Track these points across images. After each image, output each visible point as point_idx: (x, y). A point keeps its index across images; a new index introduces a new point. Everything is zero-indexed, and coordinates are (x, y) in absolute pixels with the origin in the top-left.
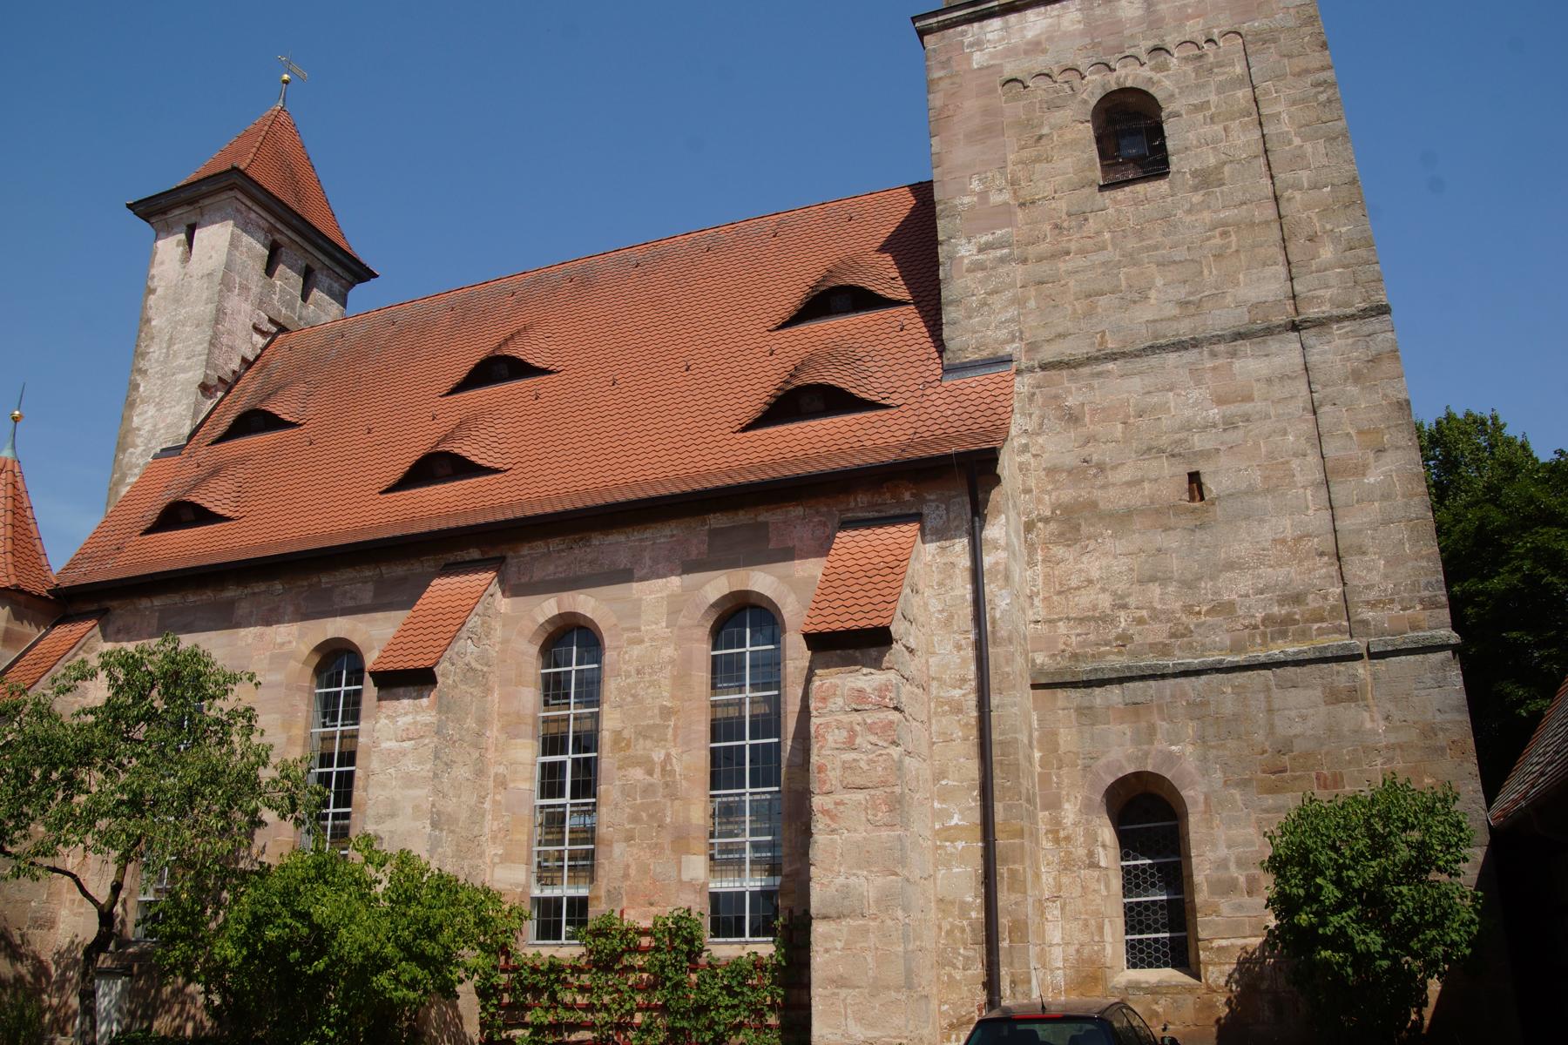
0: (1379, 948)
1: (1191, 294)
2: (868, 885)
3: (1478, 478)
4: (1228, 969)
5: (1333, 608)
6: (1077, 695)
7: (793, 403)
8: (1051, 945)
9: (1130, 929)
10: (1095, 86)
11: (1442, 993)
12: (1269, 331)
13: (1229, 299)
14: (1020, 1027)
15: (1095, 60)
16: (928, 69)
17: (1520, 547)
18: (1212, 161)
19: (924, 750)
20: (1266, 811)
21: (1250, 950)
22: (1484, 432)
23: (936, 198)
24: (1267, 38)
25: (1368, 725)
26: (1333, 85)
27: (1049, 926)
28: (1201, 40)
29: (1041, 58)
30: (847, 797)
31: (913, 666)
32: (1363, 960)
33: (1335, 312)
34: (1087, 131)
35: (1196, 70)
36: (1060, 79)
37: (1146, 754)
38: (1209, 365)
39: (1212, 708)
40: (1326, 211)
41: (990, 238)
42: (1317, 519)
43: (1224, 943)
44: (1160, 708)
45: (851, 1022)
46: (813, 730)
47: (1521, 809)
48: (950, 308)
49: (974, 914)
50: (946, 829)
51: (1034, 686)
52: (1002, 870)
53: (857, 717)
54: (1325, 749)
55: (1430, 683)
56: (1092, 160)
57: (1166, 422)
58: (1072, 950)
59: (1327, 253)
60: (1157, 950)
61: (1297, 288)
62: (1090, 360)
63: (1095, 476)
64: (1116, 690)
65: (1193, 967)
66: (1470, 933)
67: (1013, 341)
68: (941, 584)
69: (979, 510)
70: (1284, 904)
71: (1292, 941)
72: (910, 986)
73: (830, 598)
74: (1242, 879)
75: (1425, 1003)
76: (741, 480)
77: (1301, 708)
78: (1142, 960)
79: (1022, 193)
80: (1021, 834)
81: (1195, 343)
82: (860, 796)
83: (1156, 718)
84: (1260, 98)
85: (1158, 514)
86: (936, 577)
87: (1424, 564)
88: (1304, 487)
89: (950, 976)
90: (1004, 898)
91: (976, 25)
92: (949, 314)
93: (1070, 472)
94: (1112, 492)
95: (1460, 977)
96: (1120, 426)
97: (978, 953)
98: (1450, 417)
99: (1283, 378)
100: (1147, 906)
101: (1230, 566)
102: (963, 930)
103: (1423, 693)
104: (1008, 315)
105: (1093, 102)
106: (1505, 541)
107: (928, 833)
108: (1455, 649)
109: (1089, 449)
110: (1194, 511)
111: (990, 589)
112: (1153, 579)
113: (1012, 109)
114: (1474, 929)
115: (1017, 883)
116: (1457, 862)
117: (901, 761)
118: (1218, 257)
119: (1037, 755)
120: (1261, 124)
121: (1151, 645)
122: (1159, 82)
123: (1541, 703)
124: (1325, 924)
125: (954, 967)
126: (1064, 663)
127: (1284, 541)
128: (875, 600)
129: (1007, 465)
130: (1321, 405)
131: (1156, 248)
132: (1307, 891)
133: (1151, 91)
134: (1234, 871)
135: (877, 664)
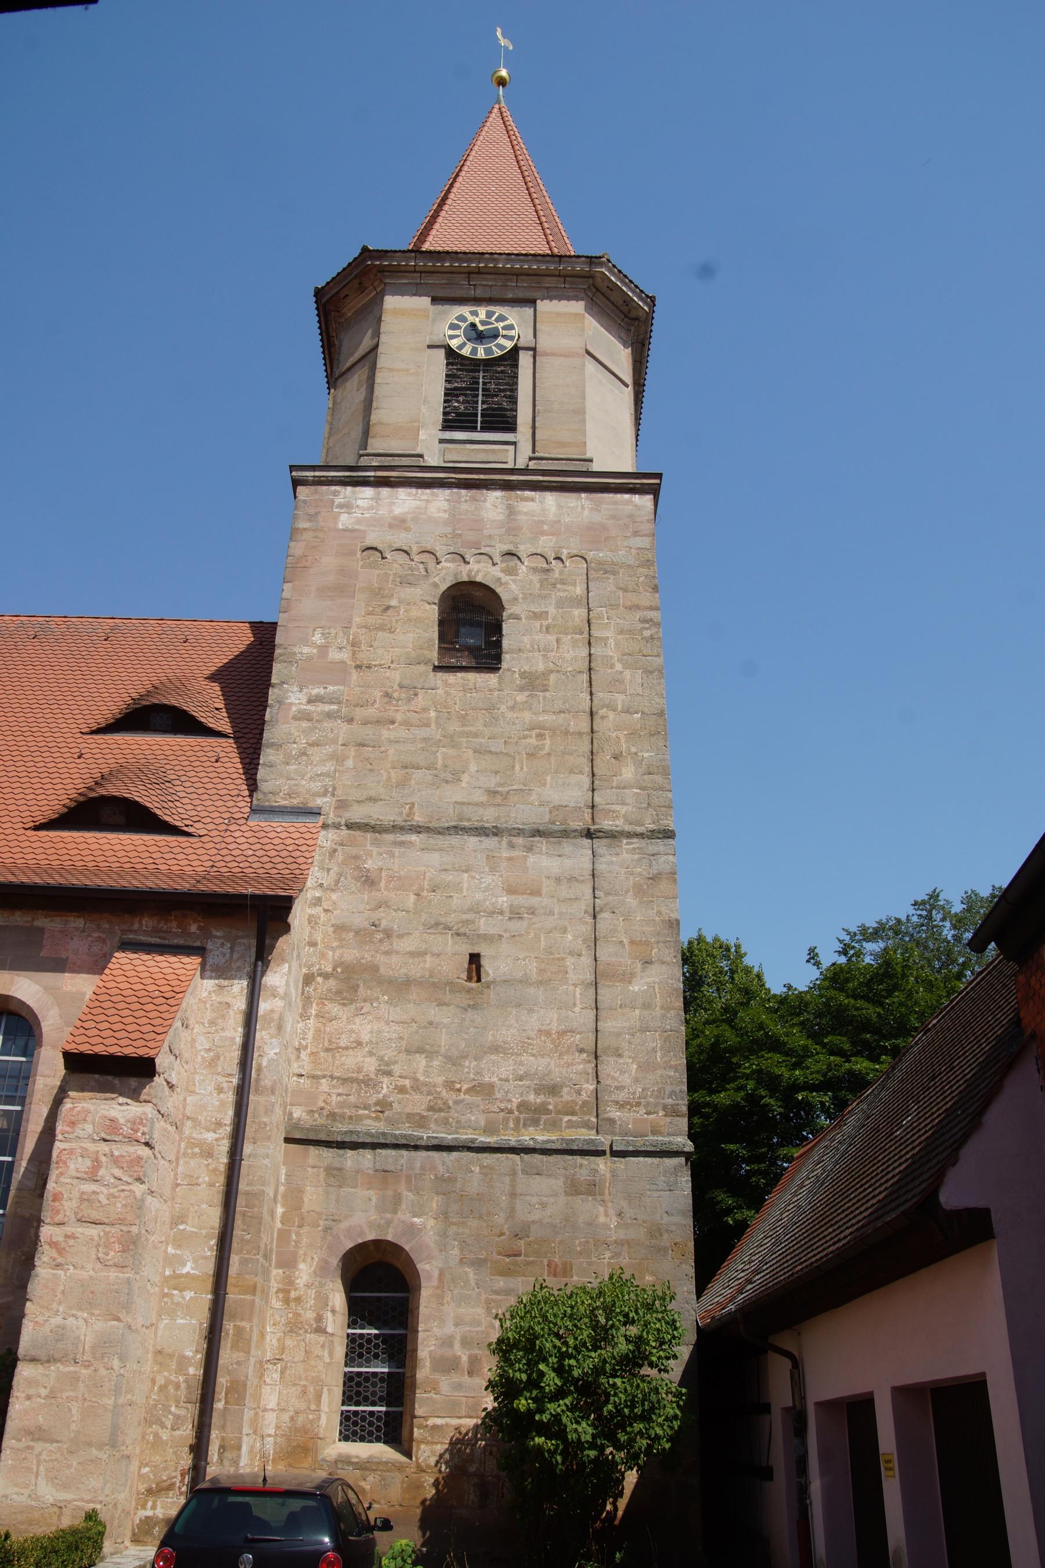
0: (589, 1438)
1: (501, 785)
2: (86, 1328)
3: (717, 998)
4: (440, 1448)
5: (585, 1103)
6: (328, 1155)
7: (99, 811)
8: (265, 1410)
9: (347, 1399)
10: (448, 574)
11: (638, 1485)
12: (566, 834)
13: (534, 797)
14: (232, 1499)
15: (452, 550)
16: (295, 517)
17: (748, 1067)
18: (541, 667)
19: (167, 1192)
20: (497, 1292)
21: (463, 1430)
22: (727, 957)
23: (278, 641)
24: (608, 569)
25: (602, 1219)
26: (658, 625)
27: (266, 1390)
28: (551, 555)
29: (403, 535)
30: (79, 1230)
31: (171, 1103)
32: (572, 1449)
33: (627, 828)
34: (432, 613)
35: (541, 582)
36: (417, 558)
37: (389, 1223)
38: (505, 854)
39: (459, 1185)
40: (633, 735)
41: (322, 691)
42: (581, 1016)
43: (439, 1421)
44: (408, 1178)
45: (42, 1481)
46: (55, 1154)
47: (730, 1313)
48: (270, 751)
49: (191, 1371)
50: (176, 1276)
51: (288, 1140)
52: (229, 1326)
53: (105, 1147)
54: (560, 1237)
55: (662, 1185)
56: (431, 640)
57: (456, 901)
58: (286, 1417)
59: (628, 772)
60: (371, 1424)
61: (597, 799)
62: (395, 828)
63: (381, 941)
64: (368, 1154)
65: (405, 1445)
66: (671, 1428)
67: (325, 795)
68: (212, 1023)
69: (262, 955)
70: (505, 1388)
71: (508, 1424)
72: (113, 1444)
73: (97, 1019)
74: (465, 1359)
75: (621, 1494)
76: (25, 880)
77: (542, 1195)
78: (355, 1433)
79: (360, 656)
80: (253, 1290)
81: (497, 832)
82: (94, 1231)
83: (402, 1188)
84: (593, 621)
85: (434, 987)
86: (209, 1015)
87: (672, 1073)
88: (575, 985)
89: (156, 1435)
90: (226, 1356)
91: (349, 489)
92: (267, 756)
93: (357, 933)
94: (394, 959)
95: (657, 1469)
96: (413, 898)
97: (189, 1413)
98: (700, 939)
99: (572, 879)
100: (367, 1377)
101: (495, 1049)
102: (177, 1386)
103: (655, 1194)
104: (325, 769)
105: (444, 587)
106: (734, 1060)
107: (157, 1279)
108: (687, 1156)
109: (380, 913)
110: (469, 991)
111: (261, 1035)
112: (420, 1050)
113: (368, 575)
114: (676, 1424)
115: (242, 1341)
116: (668, 1358)
117: (143, 1200)
118: (531, 755)
119: (280, 1210)
120: (589, 644)
121: (409, 1116)
122: (506, 583)
123: (747, 1213)
124: (541, 1411)
125: (163, 1426)
126: (321, 1121)
127: (548, 1033)
128: (144, 1029)
129: (298, 917)
130: (601, 911)
131: (476, 735)
132: (529, 1377)
133: (498, 590)
134: (458, 1350)
135: (135, 1095)
